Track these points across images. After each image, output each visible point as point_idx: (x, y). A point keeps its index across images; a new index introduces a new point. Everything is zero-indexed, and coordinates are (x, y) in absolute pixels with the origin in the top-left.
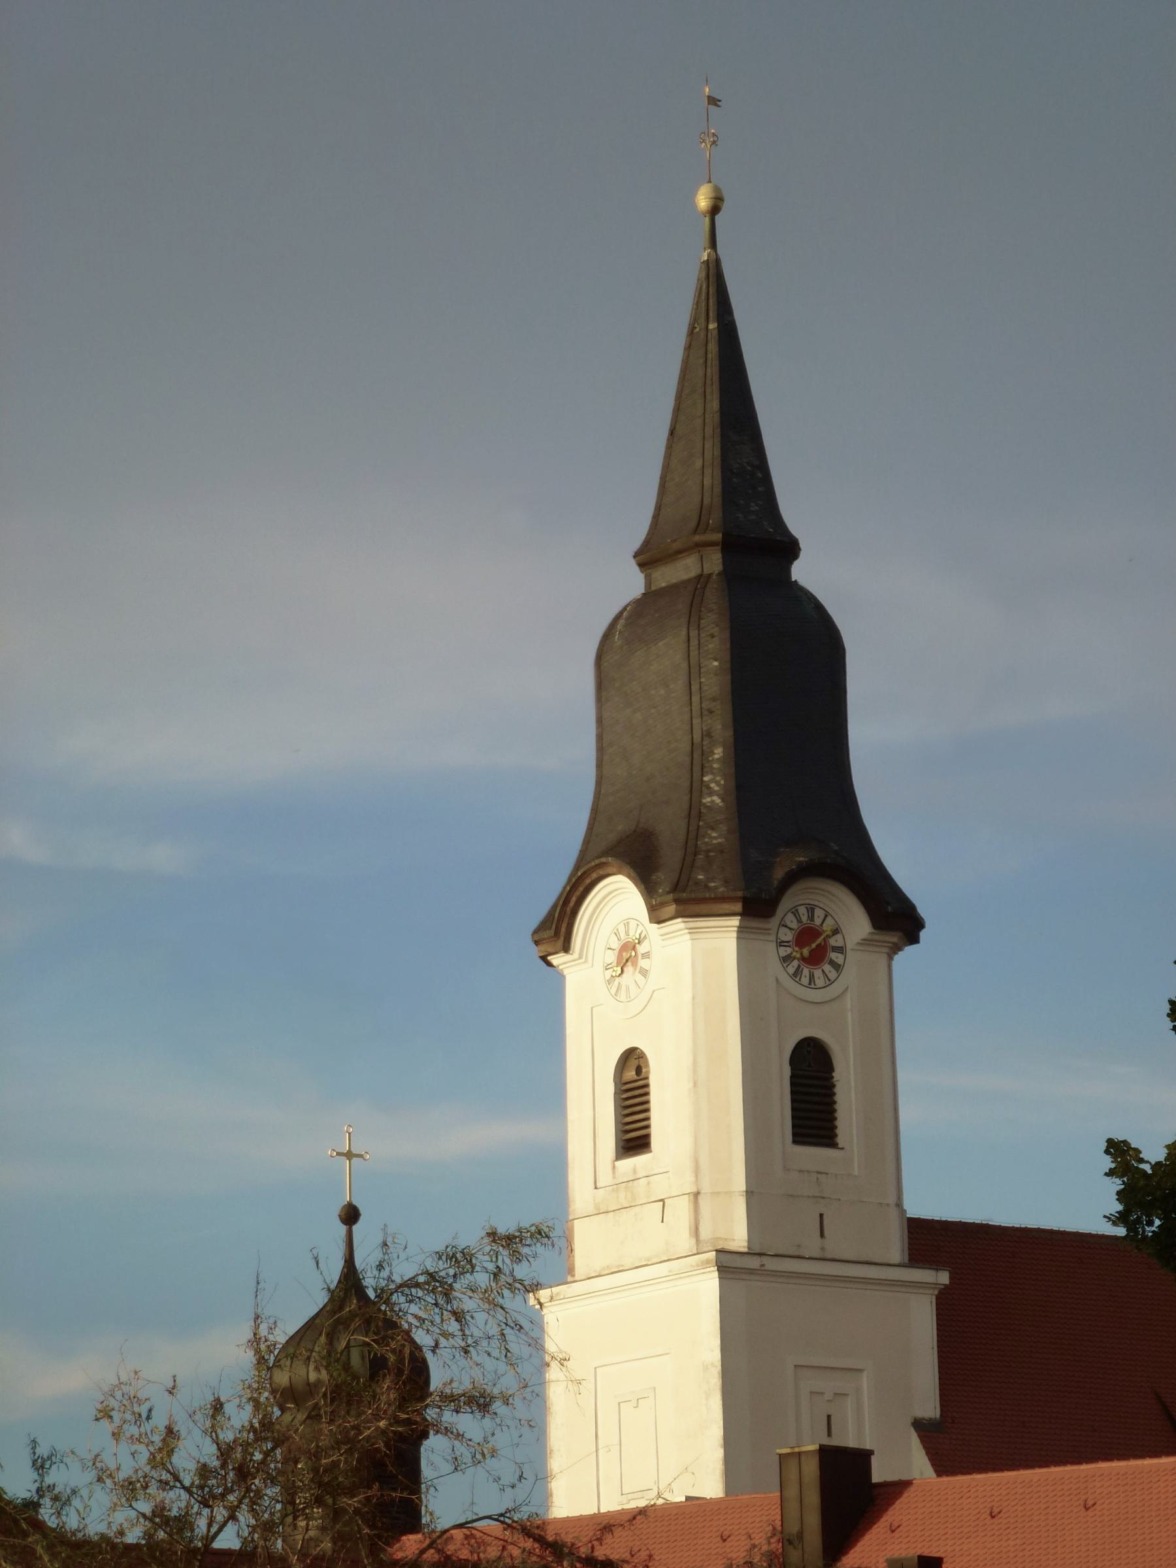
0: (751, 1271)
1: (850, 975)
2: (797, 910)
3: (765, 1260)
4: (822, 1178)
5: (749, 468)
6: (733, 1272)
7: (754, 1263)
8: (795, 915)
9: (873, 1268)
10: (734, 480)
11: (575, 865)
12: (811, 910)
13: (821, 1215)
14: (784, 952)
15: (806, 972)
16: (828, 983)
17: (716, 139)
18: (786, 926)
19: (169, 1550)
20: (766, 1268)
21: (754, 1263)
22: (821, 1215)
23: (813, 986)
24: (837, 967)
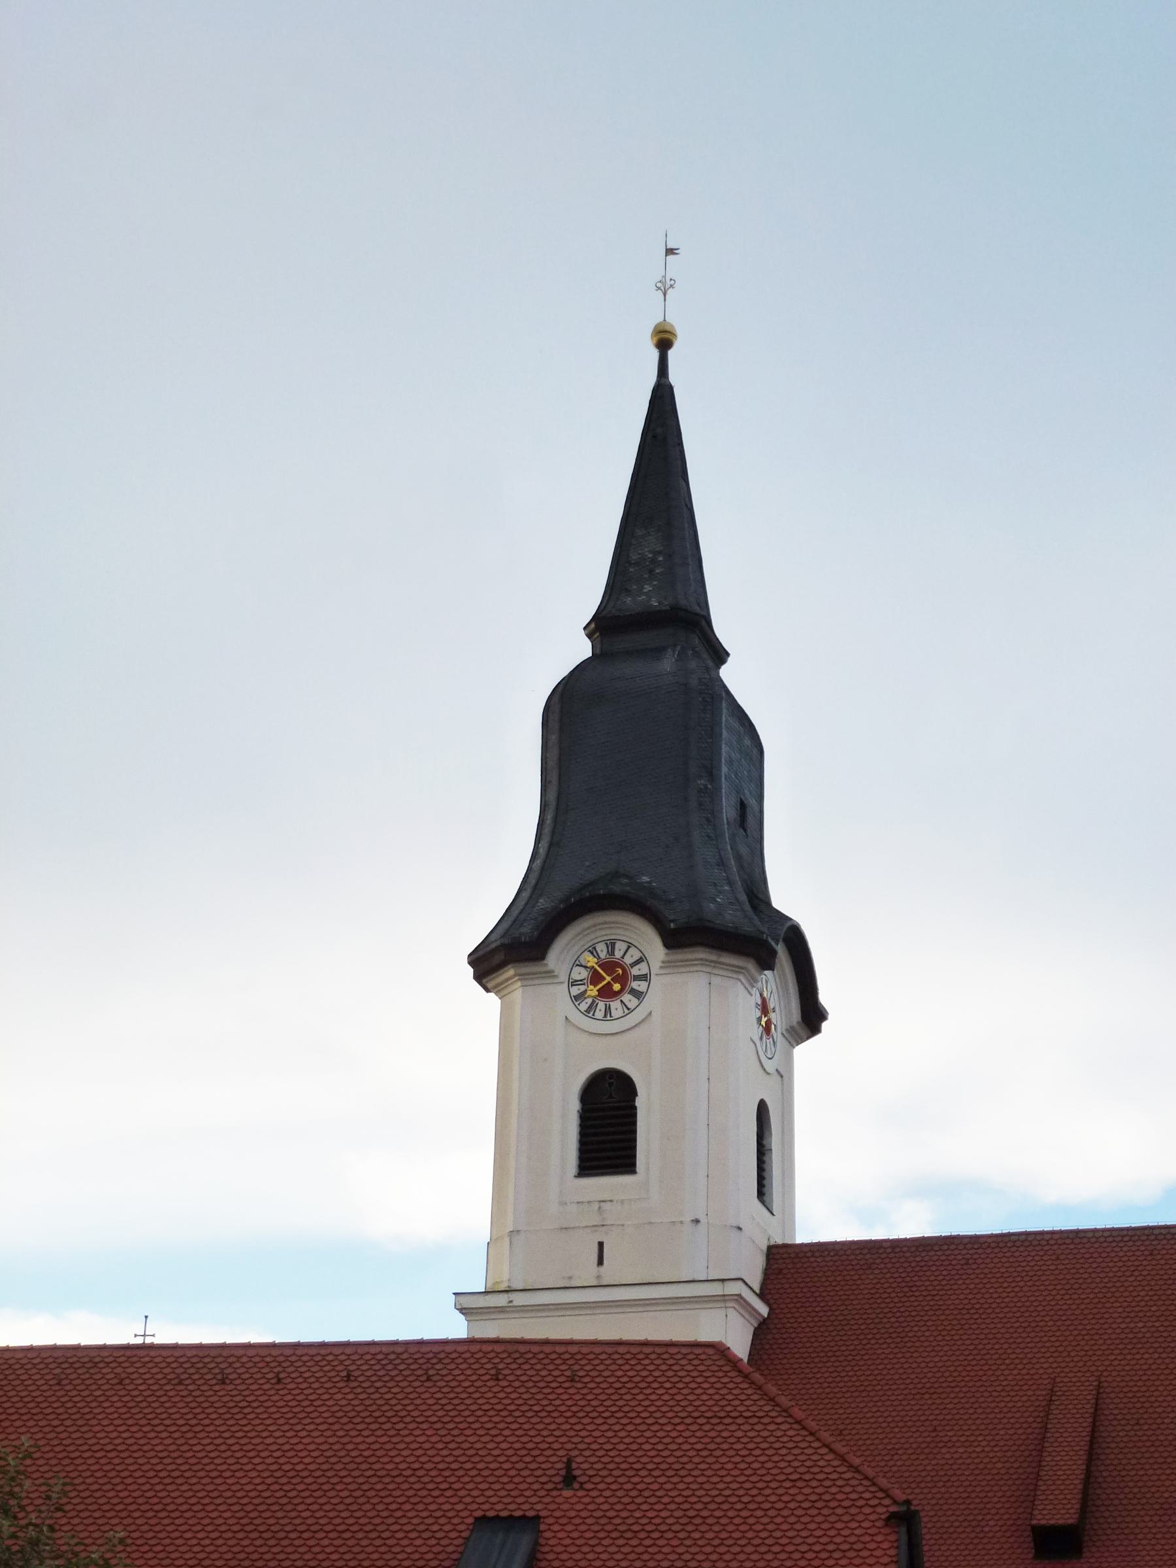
0: (501, 1310)
1: (653, 1000)
2: (595, 948)
3: (513, 1296)
4: (606, 1206)
5: (650, 556)
6: (481, 1313)
7: (501, 1300)
8: (592, 953)
9: (674, 1286)
10: (632, 570)
11: (527, 964)
12: (611, 947)
13: (601, 1245)
14: (575, 991)
15: (601, 1005)
16: (627, 1011)
17: (672, 282)
18: (581, 966)
19: (1093, 1237)
20: (515, 1303)
21: (501, 1300)
22: (601, 1245)
23: (609, 1018)
24: (638, 995)
